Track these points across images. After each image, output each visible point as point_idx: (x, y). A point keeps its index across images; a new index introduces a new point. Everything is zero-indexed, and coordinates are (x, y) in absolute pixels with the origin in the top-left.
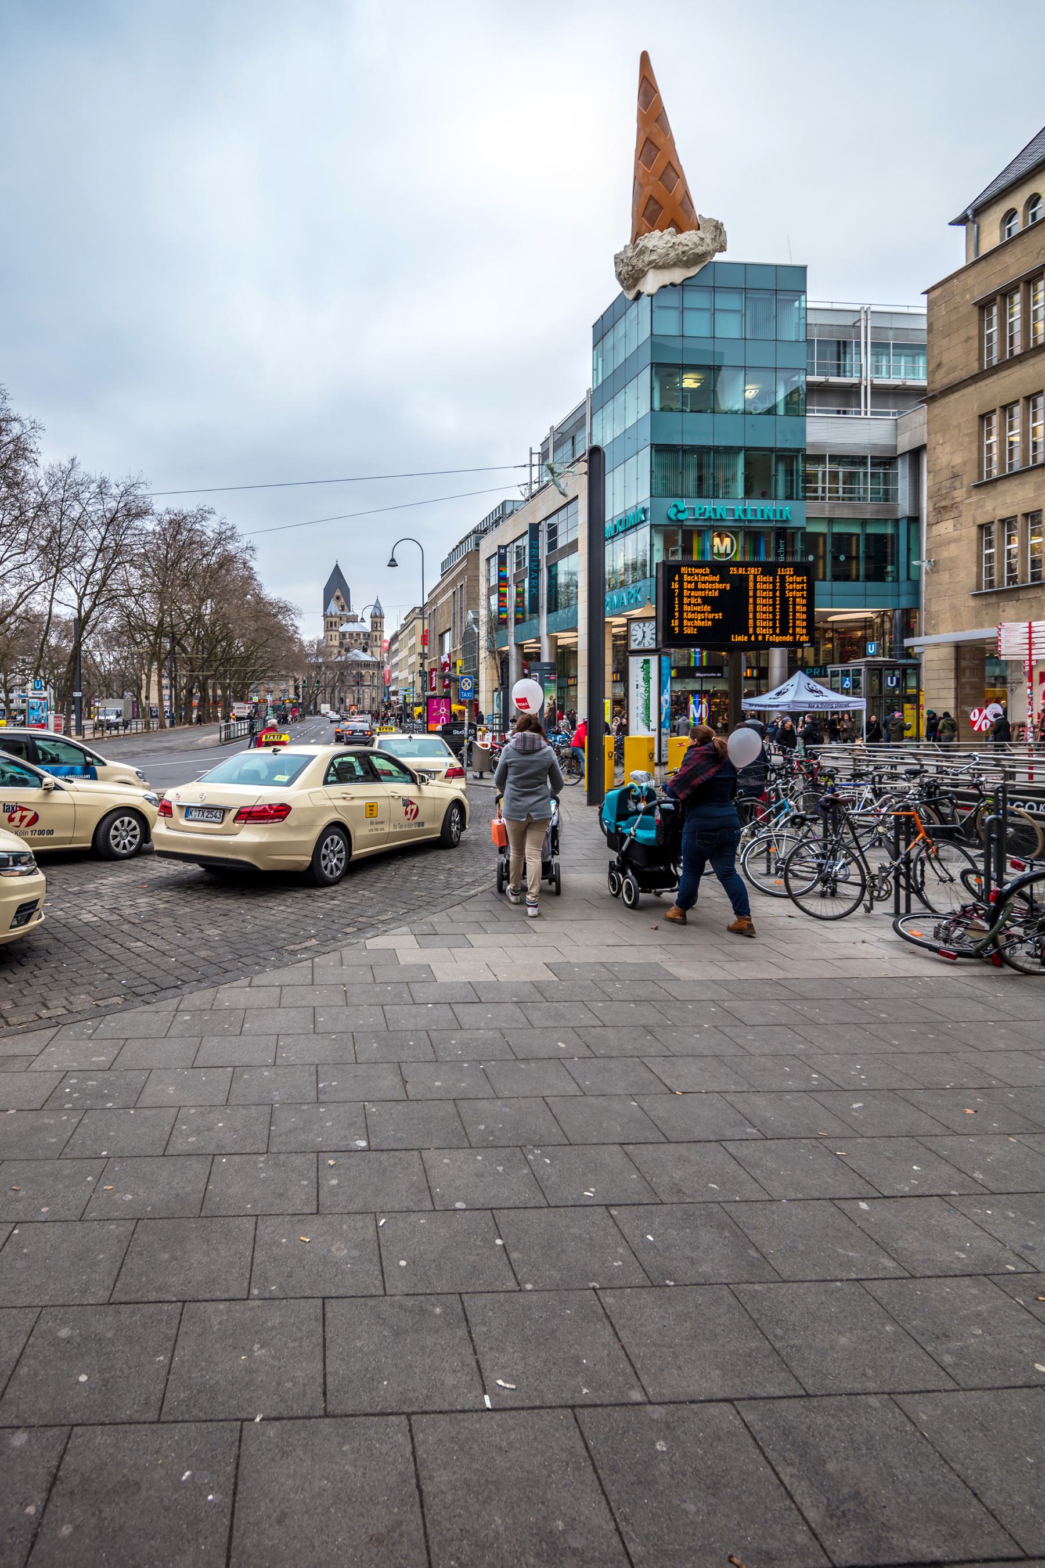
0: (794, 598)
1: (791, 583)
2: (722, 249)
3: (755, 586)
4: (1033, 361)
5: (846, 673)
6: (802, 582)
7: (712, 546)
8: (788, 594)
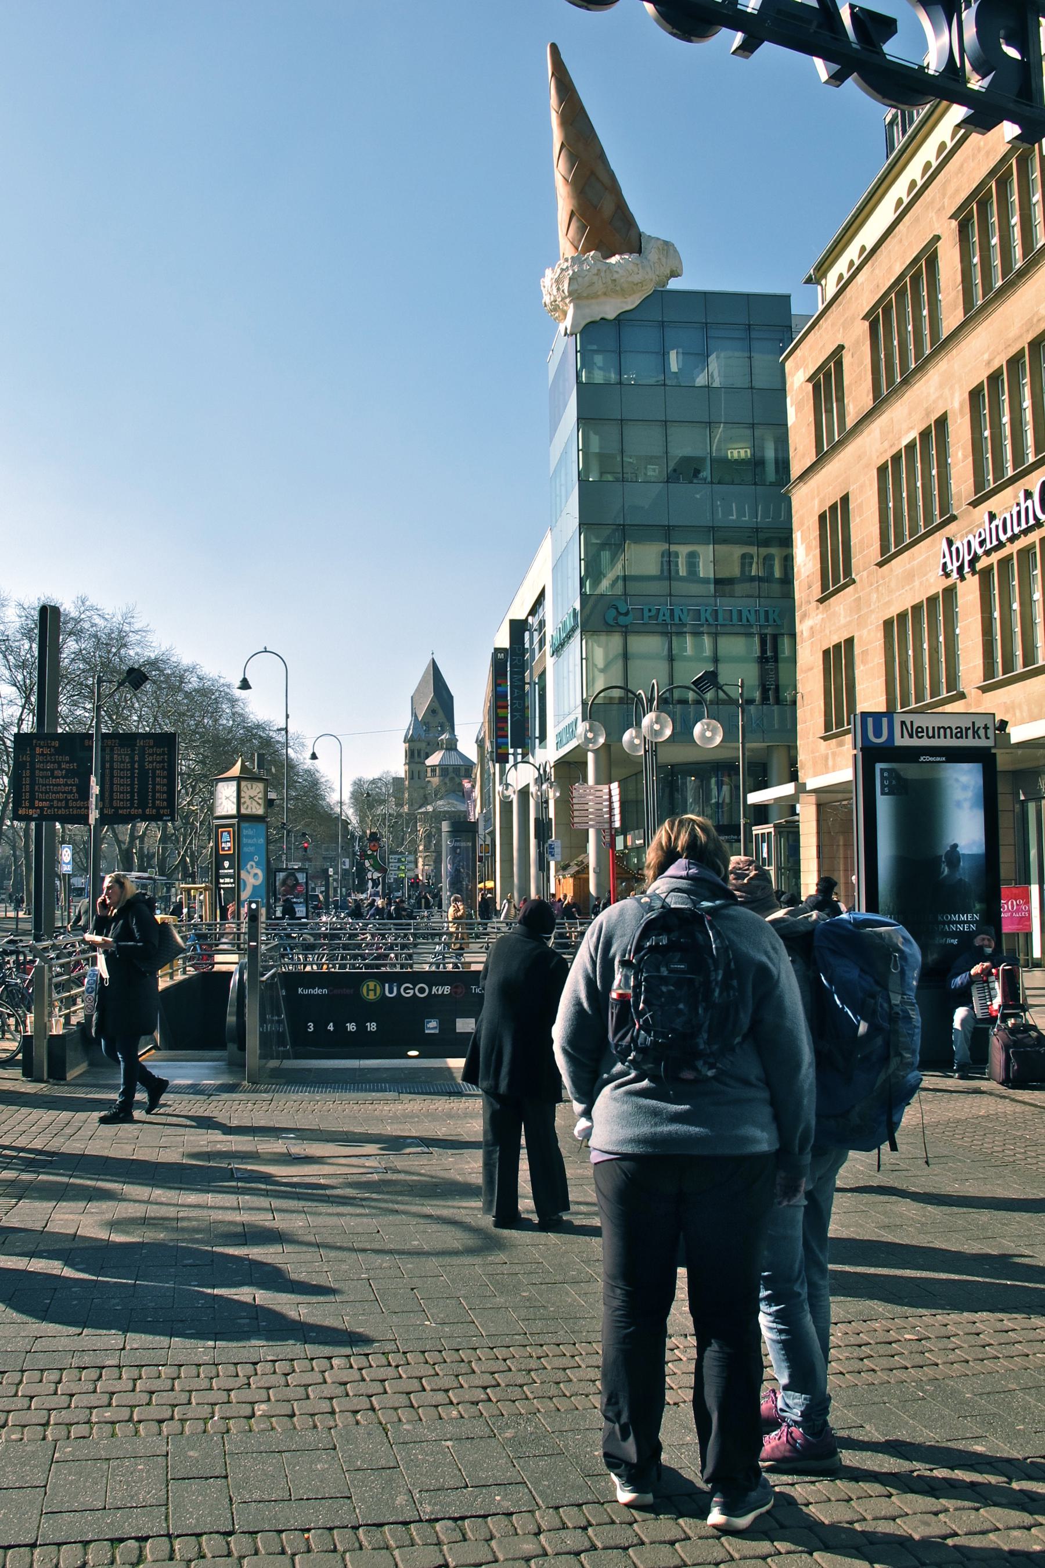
0: (154, 770)
1: (150, 755)
2: (675, 274)
3: (111, 788)
4: (959, 267)
6: (163, 754)
8: (148, 766)
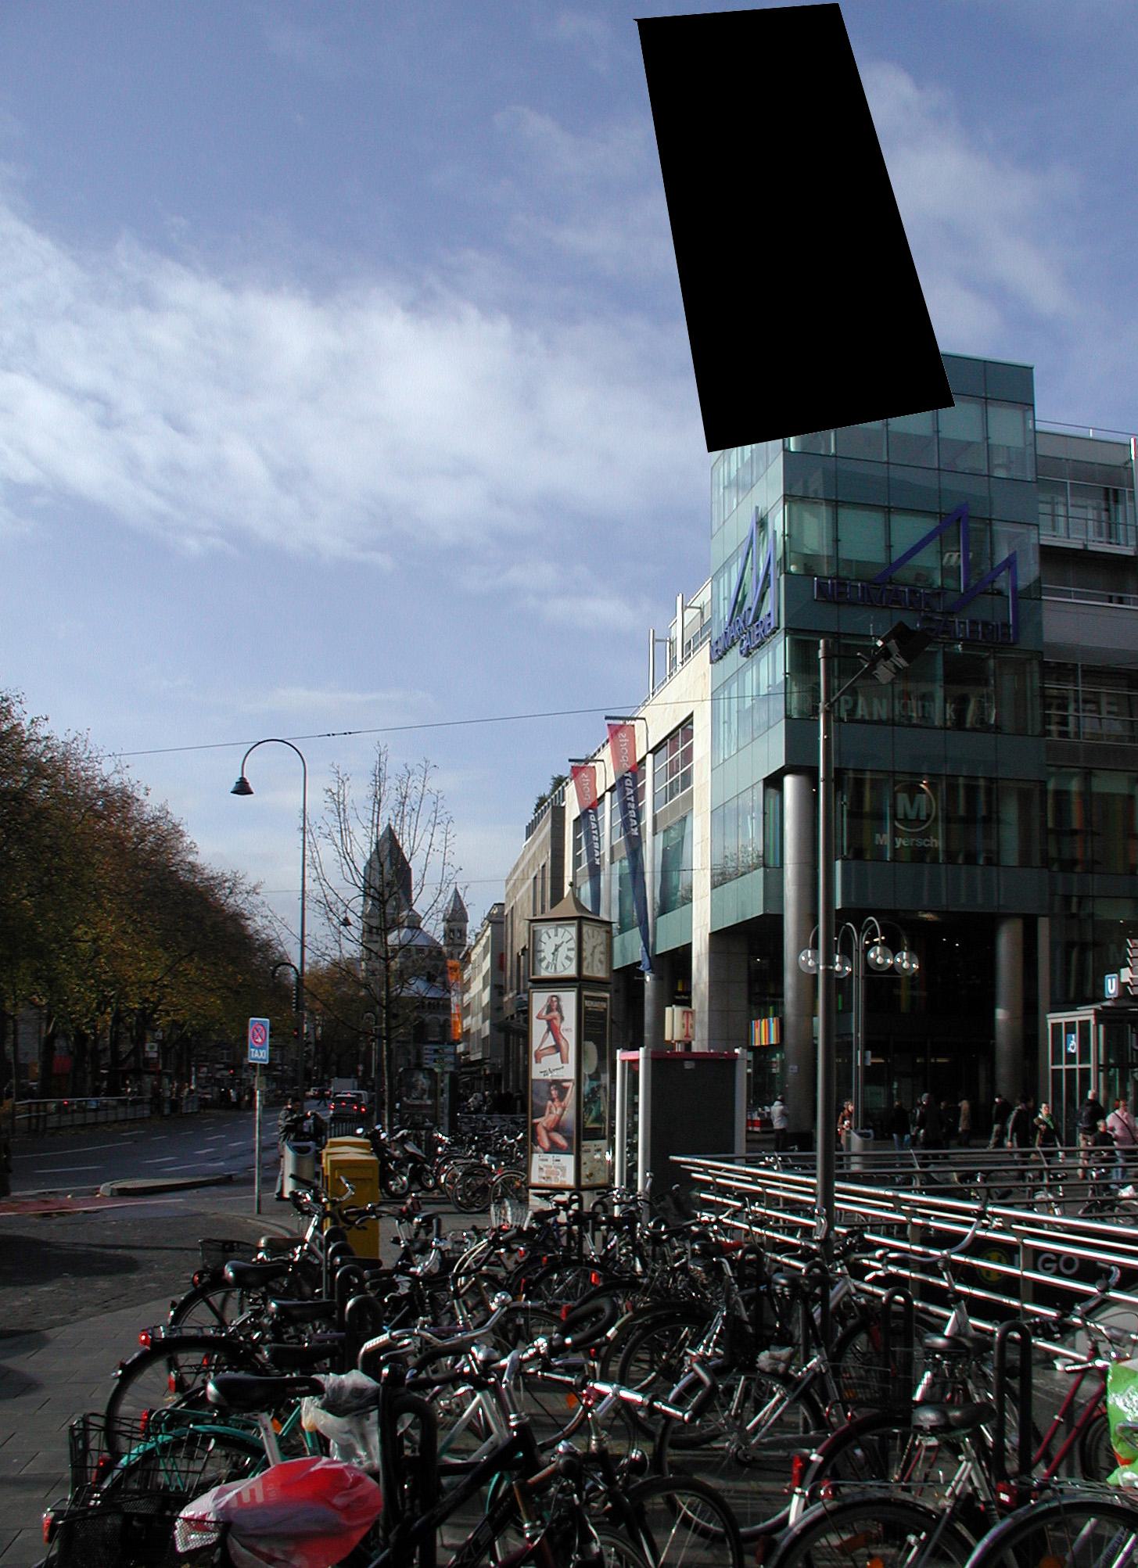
5: (1070, 1028)
7: (894, 806)
